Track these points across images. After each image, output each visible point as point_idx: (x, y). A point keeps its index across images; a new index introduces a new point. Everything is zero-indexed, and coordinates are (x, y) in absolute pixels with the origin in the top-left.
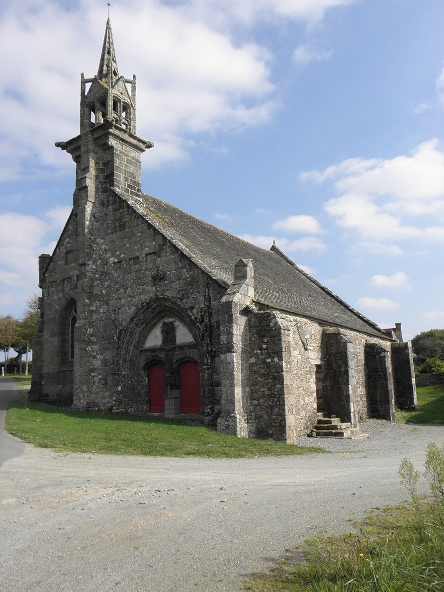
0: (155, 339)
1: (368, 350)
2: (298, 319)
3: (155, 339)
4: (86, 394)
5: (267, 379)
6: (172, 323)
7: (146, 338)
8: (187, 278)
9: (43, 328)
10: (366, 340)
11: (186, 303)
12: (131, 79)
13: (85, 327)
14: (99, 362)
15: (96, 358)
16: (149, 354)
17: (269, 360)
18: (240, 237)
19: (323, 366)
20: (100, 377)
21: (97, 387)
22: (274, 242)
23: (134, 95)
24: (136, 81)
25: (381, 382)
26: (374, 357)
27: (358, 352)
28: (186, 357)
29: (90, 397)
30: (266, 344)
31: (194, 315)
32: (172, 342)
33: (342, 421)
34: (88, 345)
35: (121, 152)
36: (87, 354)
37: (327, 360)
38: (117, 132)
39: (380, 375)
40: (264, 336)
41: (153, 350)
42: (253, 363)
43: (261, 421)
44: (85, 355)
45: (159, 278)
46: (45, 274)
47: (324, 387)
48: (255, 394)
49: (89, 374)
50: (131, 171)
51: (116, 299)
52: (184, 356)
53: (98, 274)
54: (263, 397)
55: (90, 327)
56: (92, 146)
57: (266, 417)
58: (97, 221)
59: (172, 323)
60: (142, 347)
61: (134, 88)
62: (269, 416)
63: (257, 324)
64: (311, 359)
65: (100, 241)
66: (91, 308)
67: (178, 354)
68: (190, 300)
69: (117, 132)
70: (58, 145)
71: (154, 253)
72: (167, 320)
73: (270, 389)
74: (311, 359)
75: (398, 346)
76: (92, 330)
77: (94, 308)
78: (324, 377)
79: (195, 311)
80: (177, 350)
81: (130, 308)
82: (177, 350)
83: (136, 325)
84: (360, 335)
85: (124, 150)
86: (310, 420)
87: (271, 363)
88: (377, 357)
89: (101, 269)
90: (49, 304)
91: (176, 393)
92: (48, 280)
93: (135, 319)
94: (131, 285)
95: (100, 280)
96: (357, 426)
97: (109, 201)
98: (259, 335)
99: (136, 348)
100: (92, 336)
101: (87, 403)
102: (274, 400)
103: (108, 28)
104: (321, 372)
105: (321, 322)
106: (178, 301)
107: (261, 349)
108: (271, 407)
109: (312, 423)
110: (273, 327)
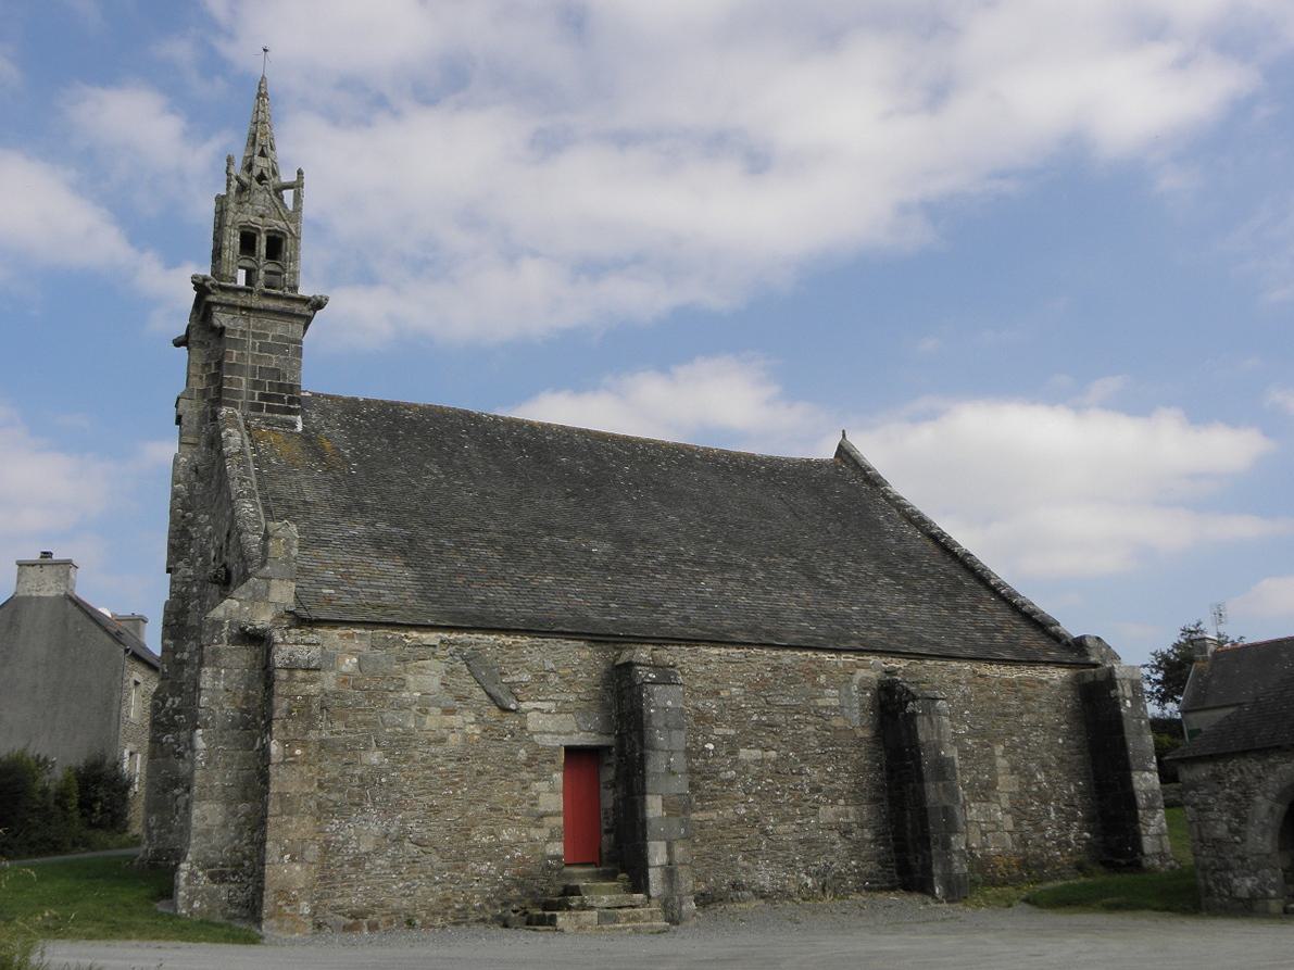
1: (883, 699)
13: (161, 695)
22: (844, 436)
24: (305, 181)
25: (911, 785)
29: (167, 839)
34: (167, 731)
36: (162, 750)
38: (230, 298)
44: (158, 753)
49: (165, 791)
50: (273, 366)
55: (171, 695)
56: (198, 333)
58: (201, 480)
61: (297, 199)
65: (203, 518)
66: (178, 656)
69: (230, 298)
75: (1092, 679)
76: (177, 700)
77: (186, 655)
85: (255, 327)
95: (198, 597)
100: (178, 711)
101: (157, 851)
105: (595, 638)
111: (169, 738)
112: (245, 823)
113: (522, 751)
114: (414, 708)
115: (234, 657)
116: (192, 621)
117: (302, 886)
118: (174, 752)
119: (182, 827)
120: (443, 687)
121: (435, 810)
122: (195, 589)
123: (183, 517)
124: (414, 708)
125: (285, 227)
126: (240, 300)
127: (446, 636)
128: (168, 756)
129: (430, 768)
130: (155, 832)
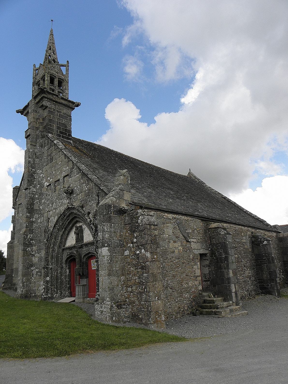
0: (71, 241)
2: (177, 216)
3: (71, 241)
4: (25, 284)
5: (137, 269)
6: (81, 227)
7: (66, 239)
8: (86, 190)
9: (14, 236)
10: (252, 233)
11: (85, 210)
12: (66, 63)
14: (37, 259)
15: (34, 256)
16: (68, 251)
17: (138, 252)
18: (95, 143)
19: (208, 255)
20: (37, 270)
21: (35, 278)
22: (190, 170)
23: (67, 74)
26: (258, 245)
27: (244, 242)
28: (90, 253)
30: (136, 238)
31: (89, 218)
32: (80, 241)
33: (225, 300)
35: (54, 110)
37: (211, 250)
39: (264, 259)
40: (134, 231)
41: (70, 248)
42: (127, 255)
43: (133, 306)
45: (70, 193)
46: (16, 199)
47: (210, 271)
48: (129, 282)
49: (28, 268)
51: (47, 212)
52: (88, 252)
53: (37, 195)
54: (135, 284)
55: (29, 233)
57: (137, 303)
59: (81, 227)
60: (64, 246)
61: (67, 70)
62: (140, 302)
63: (130, 222)
64: (195, 249)
66: (31, 220)
67: (85, 250)
68: (88, 207)
70: (18, 112)
71: (68, 175)
72: (78, 225)
73: (139, 278)
74: (195, 249)
76: (31, 235)
77: (34, 220)
78: (210, 264)
79: (91, 215)
80: (84, 247)
81: (54, 217)
82: (84, 247)
83: (58, 229)
84: (246, 228)
86: (194, 300)
87: (140, 254)
88: (261, 245)
89: (40, 191)
90: (18, 220)
91: (84, 281)
92: (18, 203)
93: (57, 226)
94: (55, 200)
96: (239, 304)
97: (46, 144)
98: (131, 230)
99: (60, 247)
100: (32, 240)
102: (142, 287)
103: (52, 35)
104: (207, 260)
106: (80, 209)
107: (133, 243)
108: (141, 293)
109: (197, 303)
110: (140, 223)
111: (29, 249)
112: (124, 284)
113: (191, 255)
114: (167, 240)
115: (116, 220)
116: (36, 207)
117: (162, 309)
118: (31, 254)
119: (35, 282)
120: (173, 233)
121: (174, 276)
122: (37, 196)
123: (32, 170)
124: (167, 240)
125: (64, 78)
126: (54, 98)
127: (175, 216)
128: (29, 255)
129: (172, 261)
130: (25, 284)
